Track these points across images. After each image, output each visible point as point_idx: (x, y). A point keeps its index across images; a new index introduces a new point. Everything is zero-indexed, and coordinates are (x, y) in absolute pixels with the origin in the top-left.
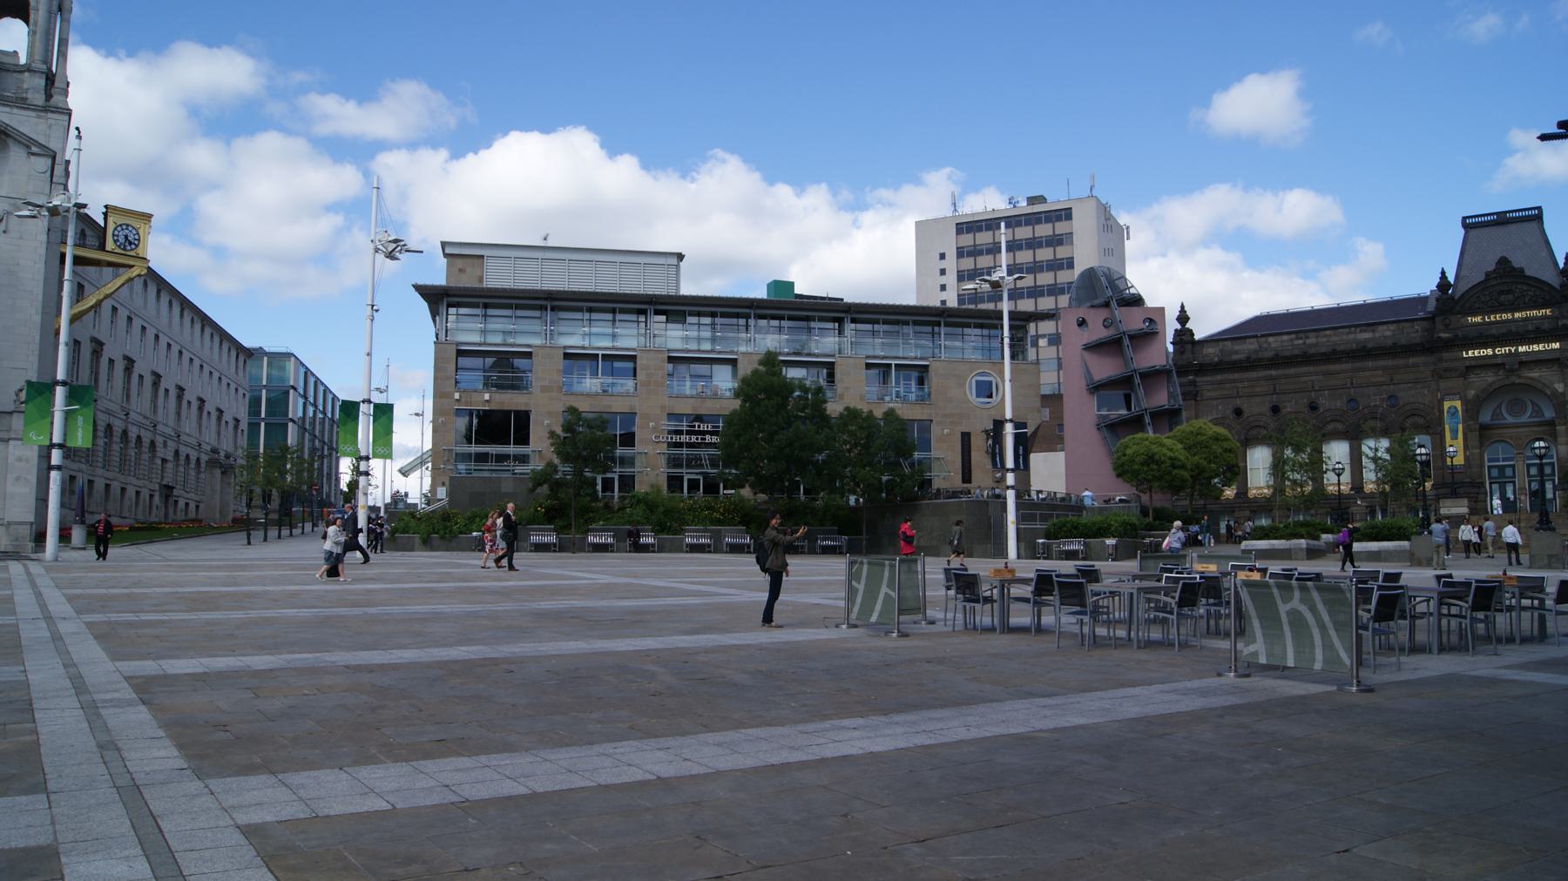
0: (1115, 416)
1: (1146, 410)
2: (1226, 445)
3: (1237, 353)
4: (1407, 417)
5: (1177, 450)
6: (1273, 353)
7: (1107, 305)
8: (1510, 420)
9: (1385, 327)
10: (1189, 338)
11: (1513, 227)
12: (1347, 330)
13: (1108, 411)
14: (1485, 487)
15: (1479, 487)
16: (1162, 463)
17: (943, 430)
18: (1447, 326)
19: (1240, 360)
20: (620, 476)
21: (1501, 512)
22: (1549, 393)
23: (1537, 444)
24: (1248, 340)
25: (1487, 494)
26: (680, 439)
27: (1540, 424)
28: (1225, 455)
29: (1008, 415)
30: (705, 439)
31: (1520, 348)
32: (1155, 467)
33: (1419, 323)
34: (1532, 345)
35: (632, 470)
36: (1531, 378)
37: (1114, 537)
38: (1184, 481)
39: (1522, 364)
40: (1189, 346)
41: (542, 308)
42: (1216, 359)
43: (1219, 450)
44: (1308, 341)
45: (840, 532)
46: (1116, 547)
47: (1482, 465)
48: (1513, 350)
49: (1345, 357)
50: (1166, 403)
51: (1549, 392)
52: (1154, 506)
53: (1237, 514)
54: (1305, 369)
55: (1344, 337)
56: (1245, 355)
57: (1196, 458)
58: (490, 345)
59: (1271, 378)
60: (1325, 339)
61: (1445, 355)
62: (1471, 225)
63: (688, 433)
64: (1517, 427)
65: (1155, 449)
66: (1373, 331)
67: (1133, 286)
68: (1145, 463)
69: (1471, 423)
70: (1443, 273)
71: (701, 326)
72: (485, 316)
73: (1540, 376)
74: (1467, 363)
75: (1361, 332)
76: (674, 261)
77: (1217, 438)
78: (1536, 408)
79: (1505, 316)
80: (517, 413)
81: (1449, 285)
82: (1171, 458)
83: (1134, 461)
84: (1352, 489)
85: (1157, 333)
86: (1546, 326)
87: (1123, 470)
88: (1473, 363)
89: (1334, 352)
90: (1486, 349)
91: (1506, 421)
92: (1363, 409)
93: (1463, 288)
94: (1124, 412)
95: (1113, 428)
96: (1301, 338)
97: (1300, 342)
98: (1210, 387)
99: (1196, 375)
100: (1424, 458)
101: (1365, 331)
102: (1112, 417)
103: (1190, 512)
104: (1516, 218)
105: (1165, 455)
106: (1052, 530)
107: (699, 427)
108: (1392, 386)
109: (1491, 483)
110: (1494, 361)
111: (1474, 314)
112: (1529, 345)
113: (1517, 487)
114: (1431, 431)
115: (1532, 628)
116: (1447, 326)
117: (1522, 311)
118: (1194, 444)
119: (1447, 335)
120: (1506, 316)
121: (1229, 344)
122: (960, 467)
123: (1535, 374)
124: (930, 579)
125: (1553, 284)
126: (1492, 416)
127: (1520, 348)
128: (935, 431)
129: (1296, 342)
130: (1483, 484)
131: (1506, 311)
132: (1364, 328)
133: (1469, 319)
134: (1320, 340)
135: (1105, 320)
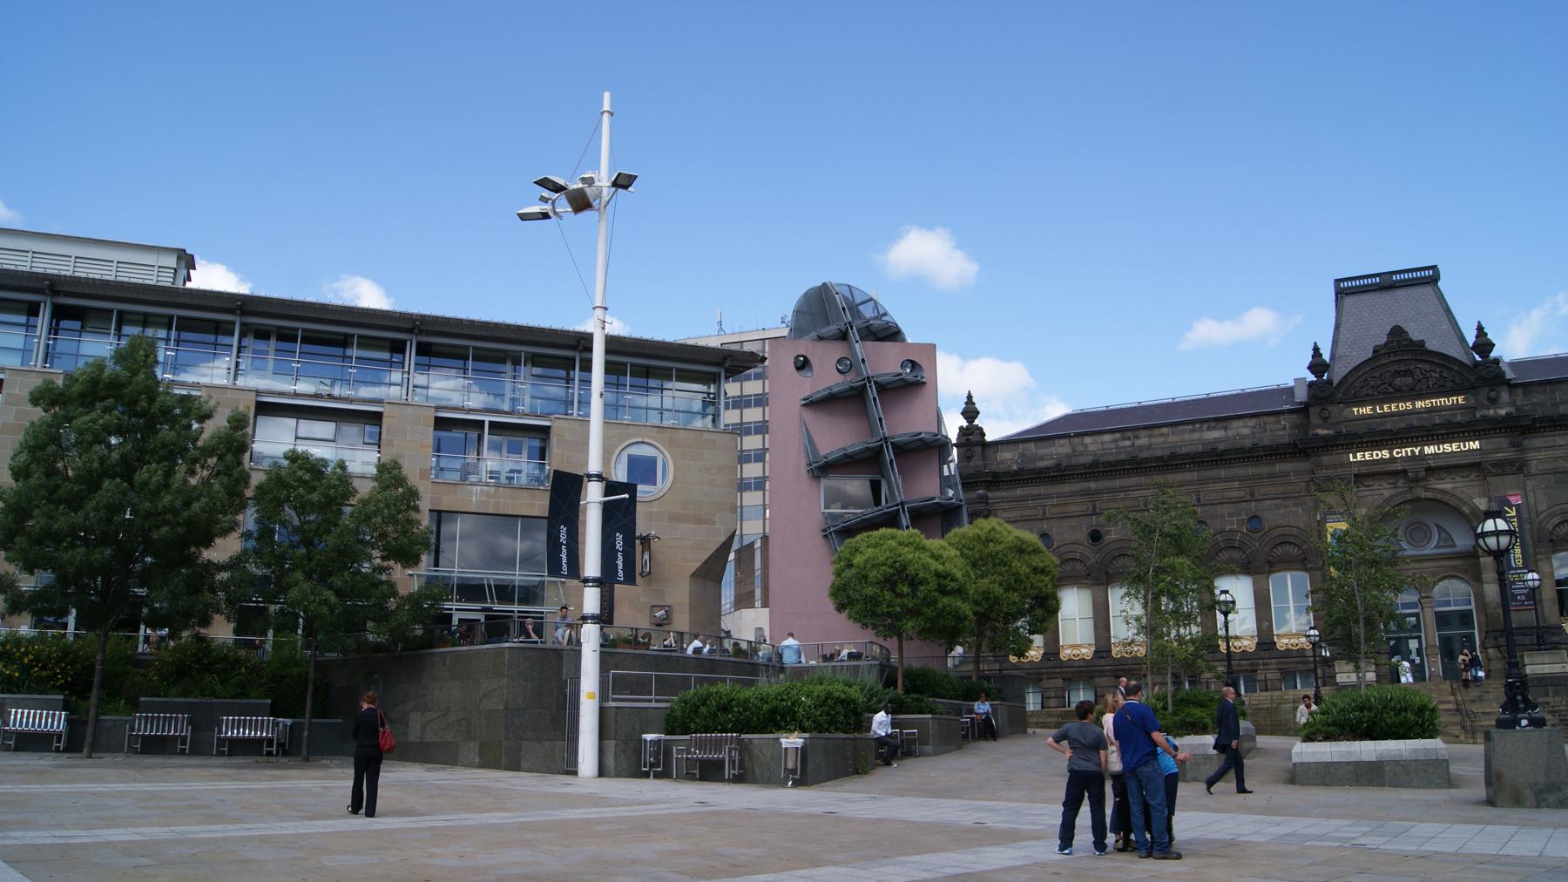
1: (902, 503)
2: (1036, 561)
3: (1042, 458)
4: (1275, 547)
5: (950, 559)
7: (843, 336)
8: (1411, 551)
9: (1241, 423)
10: (979, 438)
11: (1401, 294)
12: (1190, 427)
13: (842, 508)
16: (921, 583)
18: (1325, 419)
21: (1411, 680)
22: (1467, 512)
27: (1450, 557)
28: (1034, 578)
29: (594, 466)
31: (1426, 448)
32: (906, 589)
33: (1286, 416)
34: (1443, 443)
36: (1443, 492)
37: (804, 730)
38: (960, 618)
39: (1429, 470)
40: (978, 450)
43: (1025, 570)
44: (1138, 442)
45: (276, 711)
46: (804, 752)
48: (1417, 451)
49: (1189, 464)
50: (937, 493)
51: (1466, 509)
52: (906, 664)
53: (1045, 684)
55: (1186, 436)
56: (1055, 461)
57: (986, 581)
60: (1161, 440)
61: (1326, 459)
62: (1345, 291)
64: (1420, 561)
65: (907, 554)
66: (1226, 428)
67: (885, 314)
68: (890, 582)
70: (1316, 349)
73: (1453, 488)
74: (1355, 470)
75: (1208, 430)
77: (1021, 549)
79: (1403, 406)
82: (938, 575)
83: (865, 577)
85: (924, 383)
88: (1364, 470)
89: (1173, 456)
90: (1381, 450)
96: (1129, 438)
97: (1127, 443)
98: (1006, 505)
99: (988, 488)
101: (1214, 428)
103: (974, 679)
105: (926, 567)
106: (679, 713)
108: (1253, 503)
111: (1361, 404)
112: (1438, 444)
116: (1325, 419)
117: (1425, 399)
118: (983, 558)
119: (1326, 432)
121: (1032, 446)
123: (1446, 485)
127: (1426, 448)
129: (1122, 444)
132: (1213, 424)
133: (1355, 409)
134: (1154, 440)
135: (839, 361)
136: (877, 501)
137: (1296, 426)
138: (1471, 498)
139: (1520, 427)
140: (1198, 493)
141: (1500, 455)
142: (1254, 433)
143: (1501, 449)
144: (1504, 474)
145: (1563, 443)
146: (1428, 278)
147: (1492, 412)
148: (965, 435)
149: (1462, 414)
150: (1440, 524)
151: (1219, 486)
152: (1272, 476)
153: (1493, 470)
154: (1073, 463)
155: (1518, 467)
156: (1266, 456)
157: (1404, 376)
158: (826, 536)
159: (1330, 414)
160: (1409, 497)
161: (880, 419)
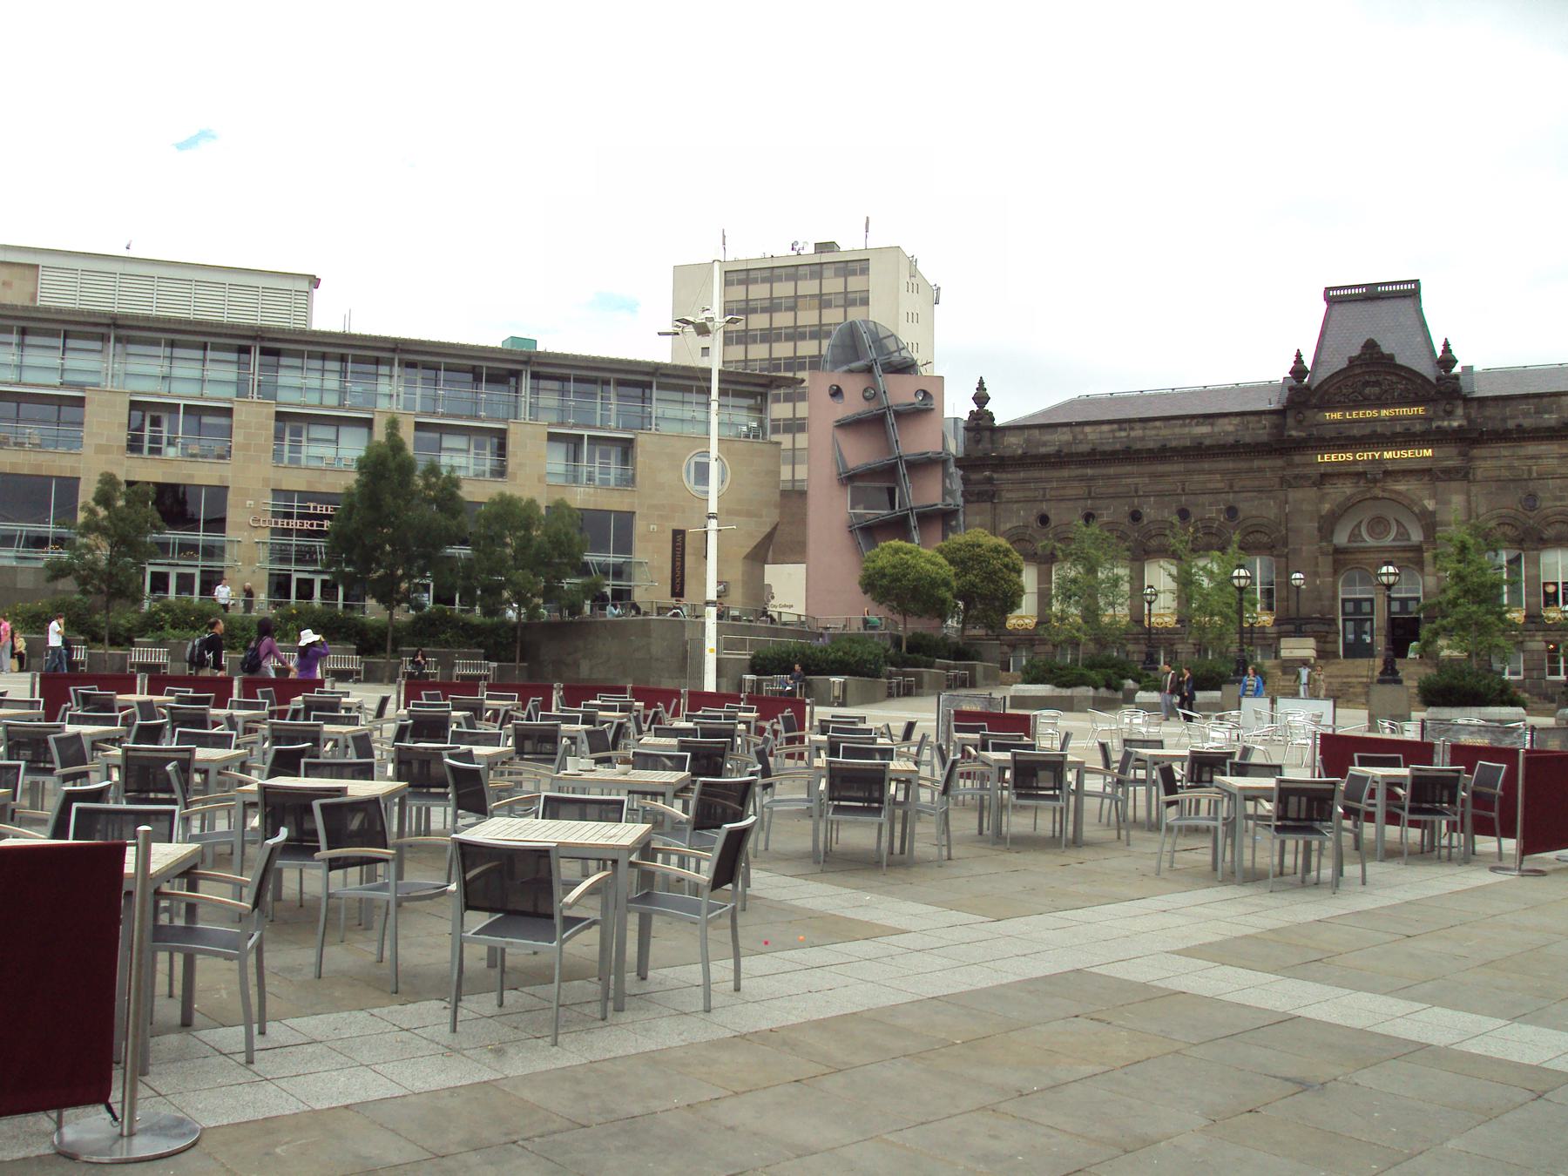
0: (872, 517)
1: (911, 509)
3: (1045, 444)
6: (1091, 446)
7: (869, 370)
8: (1370, 542)
9: (1226, 420)
12: (1181, 422)
14: (1337, 625)
15: (1329, 625)
17: (648, 525)
18: (1300, 422)
19: (1050, 455)
20: (202, 572)
22: (1417, 511)
23: (1384, 570)
24: (1059, 429)
25: (1338, 633)
26: (288, 524)
27: (1404, 549)
30: (322, 526)
33: (1268, 417)
34: (1401, 450)
35: (219, 564)
36: (1399, 493)
39: (1387, 473)
40: (987, 434)
41: (104, 338)
42: (1020, 451)
44: (1133, 434)
47: (1335, 597)
48: (1377, 456)
51: (1416, 509)
54: (1128, 469)
55: (1177, 430)
56: (1057, 448)
58: (25, 385)
59: (1082, 478)
60: (1153, 432)
61: (1297, 459)
62: (1335, 299)
63: (301, 516)
66: (1212, 425)
69: (1324, 544)
70: (1299, 355)
71: (380, 378)
72: (171, 358)
74: (1322, 470)
75: (1197, 425)
76: (304, 286)
78: (1402, 530)
80: (61, 480)
81: (1304, 372)
84: (1178, 622)
85: (932, 409)
86: (1418, 427)
87: (876, 585)
88: (1329, 470)
90: (1345, 453)
91: (1363, 544)
92: (1196, 521)
93: (1323, 374)
94: (884, 512)
95: (868, 532)
96: (1125, 430)
97: (1123, 434)
100: (1243, 582)
101: (1202, 424)
102: (868, 517)
104: (1389, 292)
107: (315, 508)
109: (1344, 620)
110: (1352, 469)
111: (1333, 409)
112: (1396, 450)
113: (1375, 626)
114: (1275, 553)
115: (1054, 831)
116: (1300, 422)
118: (963, 560)
120: (1371, 413)
121: (1036, 432)
122: (670, 575)
123: (1401, 487)
124: (930, 711)
125: (1429, 377)
126: (1350, 537)
128: (639, 527)
129: (1117, 434)
130: (1334, 621)
131: (1371, 407)
132: (1201, 420)
134: (1148, 432)
135: (865, 390)
136: (893, 506)
137: (1276, 426)
138: (1421, 500)
139: (1468, 439)
140: (1183, 483)
141: (1450, 463)
142: (1237, 430)
143: (1450, 457)
144: (1451, 480)
145: (1506, 454)
146: (1410, 293)
147: (1446, 423)
148: (975, 419)
149: (1420, 424)
150: (1401, 520)
151: (1202, 477)
152: (1251, 470)
153: (1442, 476)
154: (1074, 451)
155: (1463, 474)
156: (1245, 453)
157: (1373, 386)
158: (851, 531)
159: (1304, 417)
160: (1368, 496)
161: (897, 441)
